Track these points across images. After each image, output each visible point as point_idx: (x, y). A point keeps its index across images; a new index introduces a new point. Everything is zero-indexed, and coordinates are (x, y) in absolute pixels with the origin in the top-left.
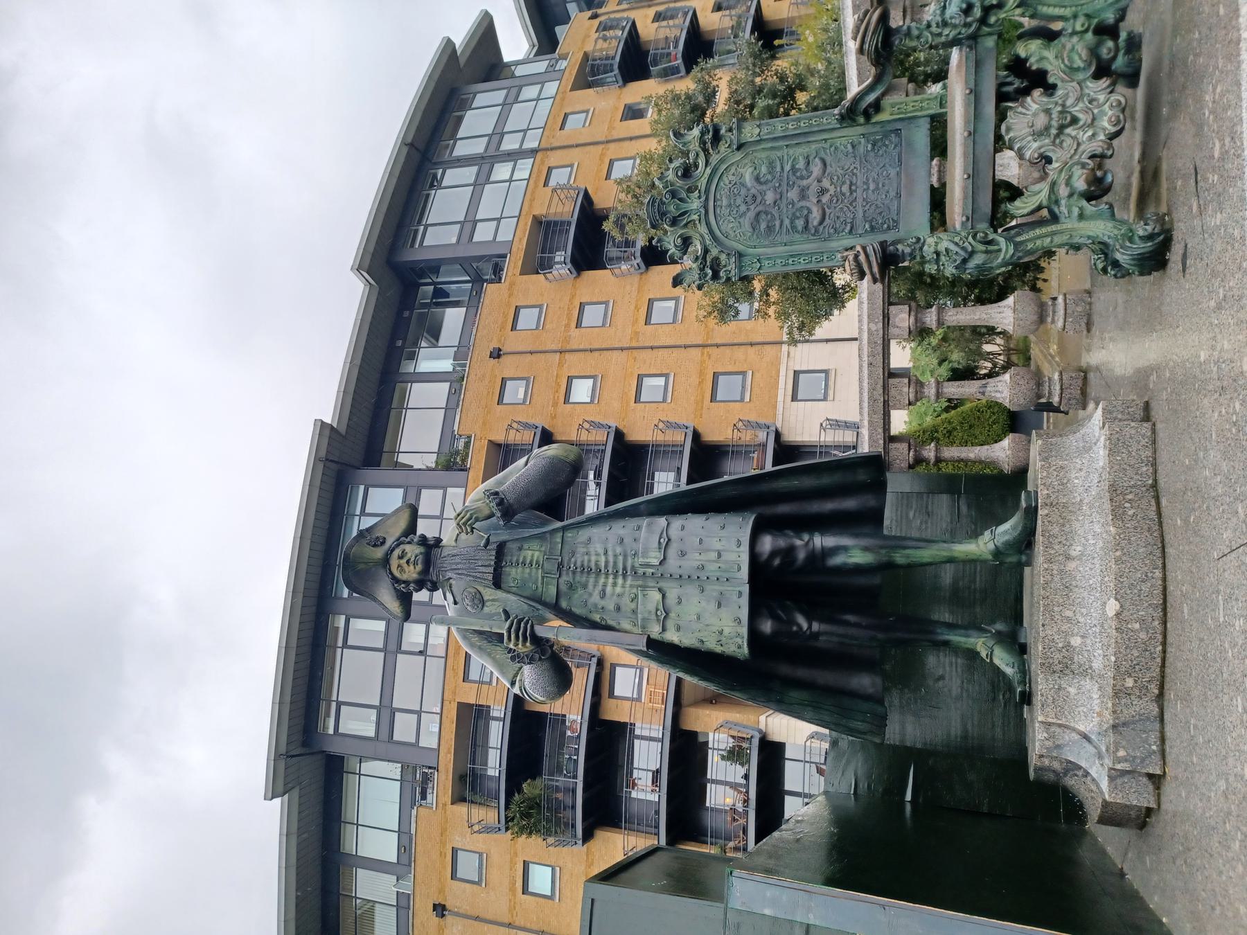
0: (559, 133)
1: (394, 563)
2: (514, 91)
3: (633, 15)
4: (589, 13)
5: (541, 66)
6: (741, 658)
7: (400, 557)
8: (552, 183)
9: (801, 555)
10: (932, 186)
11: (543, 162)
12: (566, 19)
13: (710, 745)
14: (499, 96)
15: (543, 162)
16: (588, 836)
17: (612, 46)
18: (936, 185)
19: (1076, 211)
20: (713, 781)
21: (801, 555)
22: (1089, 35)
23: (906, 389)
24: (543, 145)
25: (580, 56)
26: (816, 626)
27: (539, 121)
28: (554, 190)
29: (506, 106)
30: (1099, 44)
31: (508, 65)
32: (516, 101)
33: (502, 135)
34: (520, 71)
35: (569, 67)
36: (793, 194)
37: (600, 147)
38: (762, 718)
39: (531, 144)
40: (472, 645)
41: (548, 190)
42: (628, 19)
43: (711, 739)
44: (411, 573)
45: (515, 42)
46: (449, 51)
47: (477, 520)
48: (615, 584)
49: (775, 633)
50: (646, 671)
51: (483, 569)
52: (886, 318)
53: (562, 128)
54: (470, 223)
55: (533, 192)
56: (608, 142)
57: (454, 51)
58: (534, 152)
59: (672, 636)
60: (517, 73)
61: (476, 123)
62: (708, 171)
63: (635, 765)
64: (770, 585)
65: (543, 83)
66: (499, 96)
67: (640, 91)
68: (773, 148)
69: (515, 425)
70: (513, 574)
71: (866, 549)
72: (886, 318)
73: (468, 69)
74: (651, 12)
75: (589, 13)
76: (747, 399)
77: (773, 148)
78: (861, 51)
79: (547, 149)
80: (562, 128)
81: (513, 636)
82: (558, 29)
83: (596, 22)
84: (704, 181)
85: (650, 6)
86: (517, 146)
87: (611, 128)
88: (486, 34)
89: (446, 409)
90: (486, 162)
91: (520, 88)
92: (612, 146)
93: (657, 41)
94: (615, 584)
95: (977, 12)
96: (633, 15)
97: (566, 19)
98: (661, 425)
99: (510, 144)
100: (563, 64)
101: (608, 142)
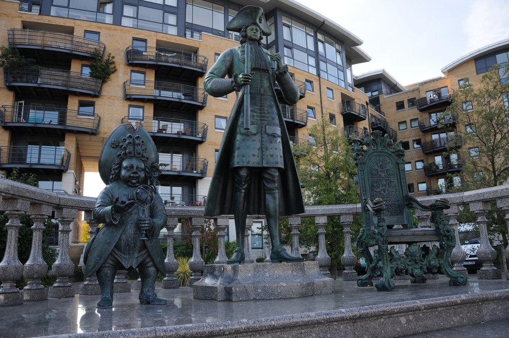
0: (326, 86)
1: (254, 27)
2: (342, 68)
3: (367, 119)
4: (368, 102)
5: (350, 80)
6: (231, 163)
7: (256, 30)
8: (307, 83)
9: (270, 186)
10: (393, 226)
11: (315, 79)
12: (366, 91)
13: (57, 147)
14: (339, 62)
15: (315, 79)
16: (10, 88)
17: (357, 110)
18: (503, 209)
19: (393, 266)
20: (40, 148)
21: (270, 186)
22: (438, 265)
23: (297, 223)
24: (321, 79)
25: (353, 97)
26: (243, 191)
27: (332, 79)
28: (304, 83)
29: (336, 65)
30: (436, 268)
31: (350, 66)
32: (338, 69)
33: (326, 63)
34: (348, 72)
35: (350, 92)
36: (384, 182)
37: (320, 104)
38: (73, 171)
39: (323, 75)
40: (225, 56)
41: (304, 81)
42: (366, 117)
43: (61, 147)
44: (250, 33)
45: (360, 70)
46: (359, 43)
47: (278, 63)
48: (257, 116)
49: (241, 177)
50: (93, 118)
51: (259, 64)
52: (323, 215)
53: (328, 88)
54: (291, 46)
55: (303, 74)
56: (322, 107)
57: (359, 45)
58: (319, 75)
59: (239, 137)
60: (347, 70)
61: (331, 51)
62: (390, 153)
63: (46, 112)
64: (258, 173)
65: (344, 81)
66: (339, 62)
67: (340, 119)
68: (397, 174)
69: (206, 60)
70: (257, 75)
71: (275, 209)
72: (323, 215)
73: (350, 50)
74: (367, 127)
75: (368, 102)
76: (216, 130)
77: (397, 174)
78: (437, 201)
79: (320, 81)
80: (328, 88)
81: (247, 77)
82: (363, 88)
83: (365, 104)
84: (387, 151)
85: (369, 126)
86: (321, 68)
87: (327, 108)
88: (362, 58)
89: (212, 29)
90: (316, 55)
91: (343, 71)
92: (320, 109)
93: (357, 128)
94: (257, 116)
95: (448, 234)
96: (367, 119)
97: (366, 91)
98: (206, 127)
99: (322, 65)
100: (350, 89)
101: (322, 107)
